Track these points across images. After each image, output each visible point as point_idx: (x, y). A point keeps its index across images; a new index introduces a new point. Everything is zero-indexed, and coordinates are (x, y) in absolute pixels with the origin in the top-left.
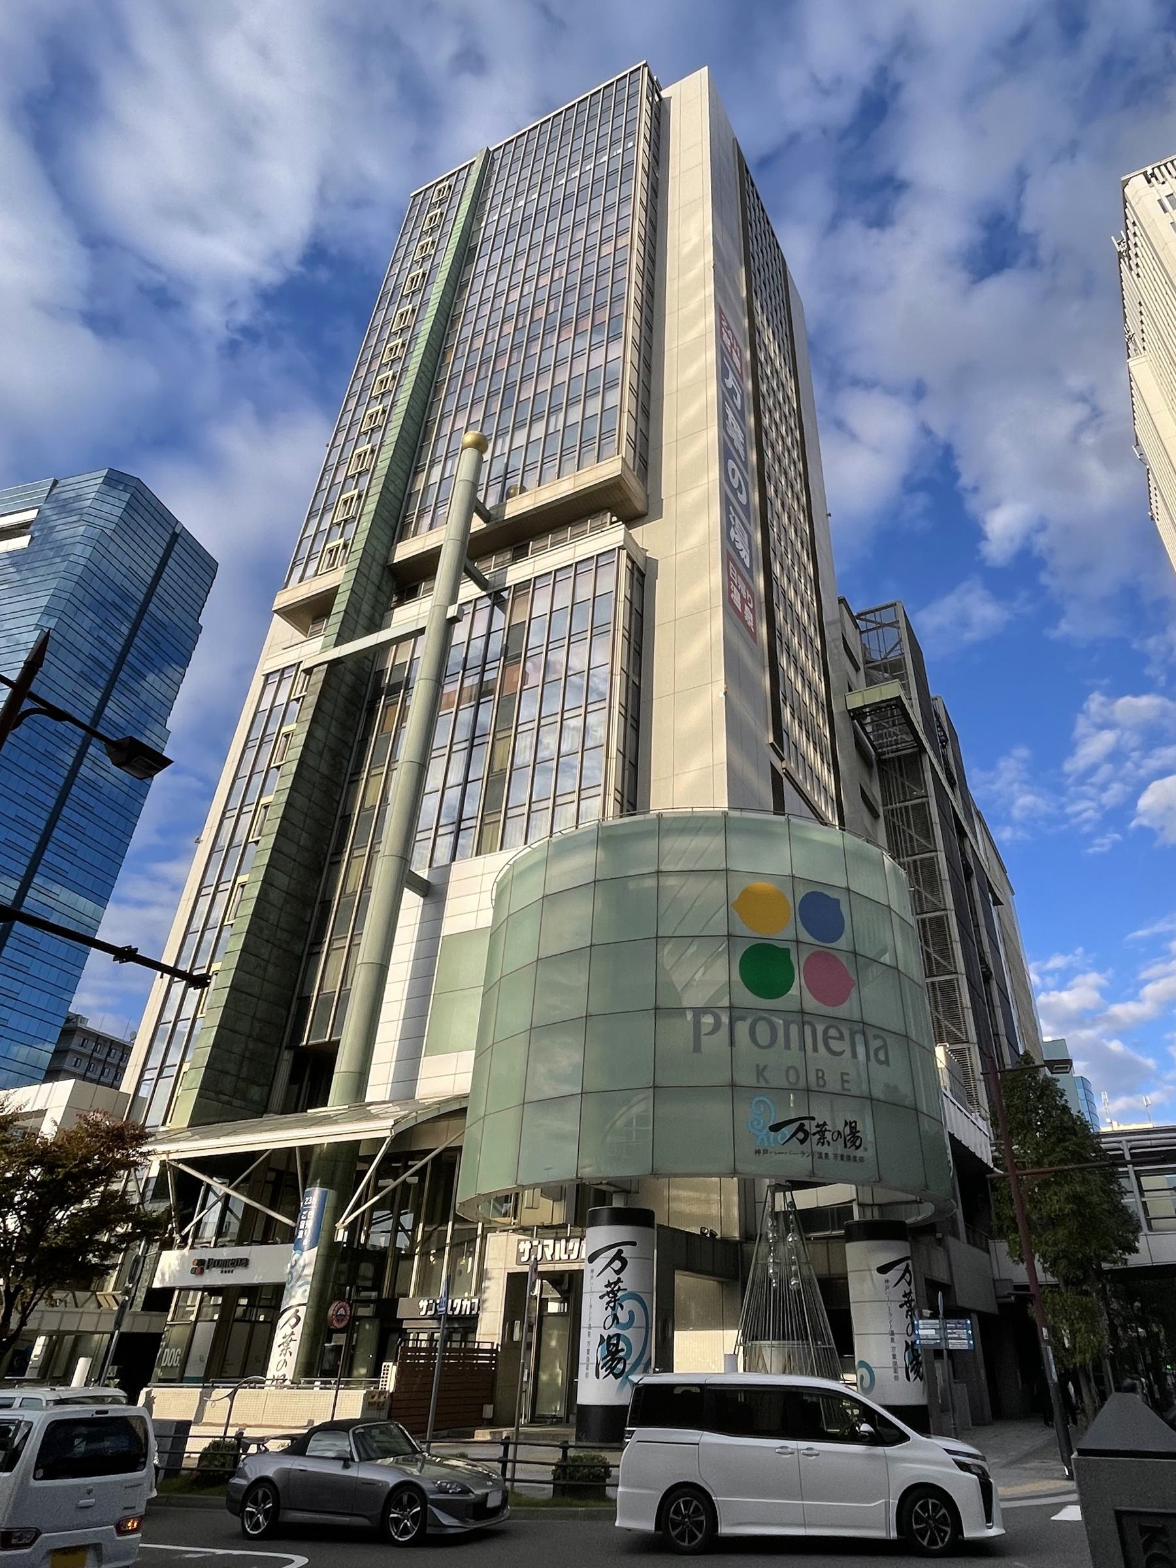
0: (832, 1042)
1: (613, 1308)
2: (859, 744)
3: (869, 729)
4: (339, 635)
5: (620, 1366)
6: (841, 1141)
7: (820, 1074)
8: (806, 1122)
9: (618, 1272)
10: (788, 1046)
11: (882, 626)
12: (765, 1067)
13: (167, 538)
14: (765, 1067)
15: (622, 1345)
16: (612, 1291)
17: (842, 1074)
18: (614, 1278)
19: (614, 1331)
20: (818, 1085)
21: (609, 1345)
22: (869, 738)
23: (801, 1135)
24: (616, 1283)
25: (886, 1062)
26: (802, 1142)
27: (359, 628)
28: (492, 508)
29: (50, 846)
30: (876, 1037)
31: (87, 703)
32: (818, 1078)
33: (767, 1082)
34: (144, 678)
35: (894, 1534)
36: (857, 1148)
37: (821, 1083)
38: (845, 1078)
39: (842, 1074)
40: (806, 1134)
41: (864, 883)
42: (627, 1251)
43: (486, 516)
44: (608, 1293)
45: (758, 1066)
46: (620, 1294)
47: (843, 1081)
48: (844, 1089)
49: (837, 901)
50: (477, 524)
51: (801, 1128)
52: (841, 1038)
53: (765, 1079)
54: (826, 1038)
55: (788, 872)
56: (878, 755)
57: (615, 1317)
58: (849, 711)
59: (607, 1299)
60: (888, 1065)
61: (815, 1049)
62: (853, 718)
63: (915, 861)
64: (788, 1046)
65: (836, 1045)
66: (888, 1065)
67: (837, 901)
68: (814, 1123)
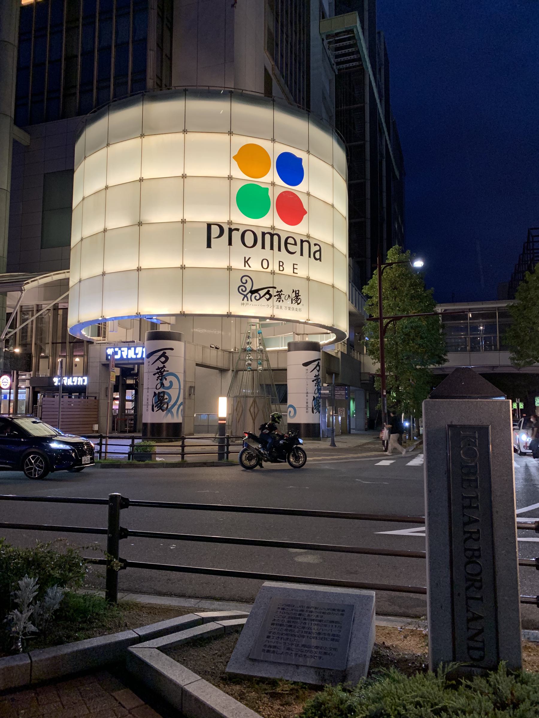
1: (161, 380)
5: (165, 406)
6: (290, 300)
7: (281, 264)
8: (271, 289)
9: (163, 363)
10: (263, 247)
15: (166, 396)
16: (160, 372)
18: (162, 365)
19: (162, 390)
21: (159, 396)
23: (163, 359)
24: (162, 368)
26: (268, 300)
30: (315, 245)
33: (250, 267)
36: (298, 304)
37: (281, 268)
40: (271, 296)
42: (168, 353)
44: (158, 373)
46: (164, 373)
51: (268, 293)
52: (295, 244)
54: (286, 243)
57: (162, 384)
59: (157, 375)
61: (279, 250)
65: (291, 248)
68: (275, 290)
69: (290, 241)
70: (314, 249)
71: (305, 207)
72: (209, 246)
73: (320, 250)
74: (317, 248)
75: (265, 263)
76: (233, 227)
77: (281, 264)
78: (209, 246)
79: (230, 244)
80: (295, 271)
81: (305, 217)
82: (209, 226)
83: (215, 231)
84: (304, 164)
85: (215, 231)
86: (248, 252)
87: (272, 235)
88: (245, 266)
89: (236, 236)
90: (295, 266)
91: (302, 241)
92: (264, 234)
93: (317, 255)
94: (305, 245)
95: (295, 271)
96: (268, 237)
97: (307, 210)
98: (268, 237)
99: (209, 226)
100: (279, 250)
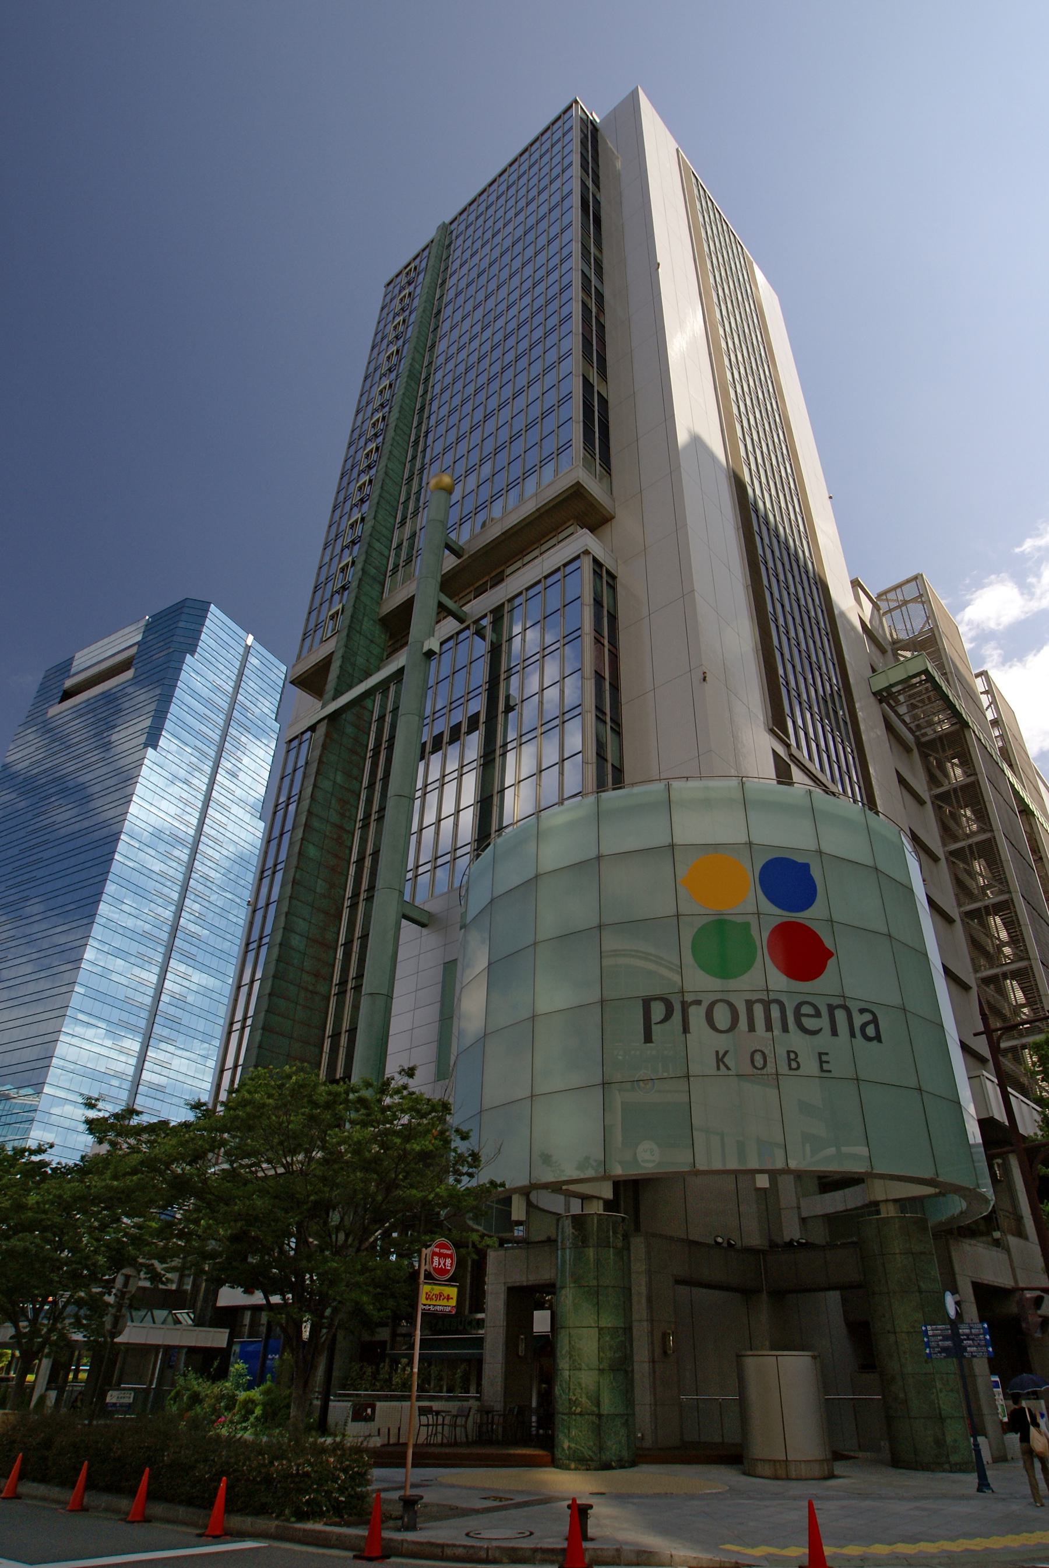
0: (805, 1021)
2: (889, 727)
3: (902, 710)
4: (336, 689)
7: (792, 1056)
10: (752, 1028)
11: (905, 603)
12: (726, 1052)
13: (241, 650)
14: (726, 1052)
17: (820, 1054)
20: (791, 1069)
22: (904, 722)
25: (878, 1038)
27: (356, 680)
28: (465, 543)
29: (169, 975)
30: (862, 1011)
31: (187, 824)
32: (789, 1060)
33: (728, 1068)
34: (110, 743)
35: (228, 1331)
37: (794, 1065)
38: (824, 1058)
39: (820, 1054)
41: (835, 842)
43: (456, 552)
45: (717, 1052)
47: (821, 1062)
48: (822, 1070)
49: (806, 866)
50: (450, 562)
52: (818, 1014)
53: (724, 1063)
55: (744, 839)
56: (917, 738)
58: (874, 694)
60: (880, 1041)
61: (785, 1029)
62: (880, 702)
63: (970, 846)
64: (752, 1028)
65: (809, 1023)
66: (880, 1041)
67: (806, 866)
69: (806, 1009)
70: (859, 1020)
71: (828, 943)
72: (648, 1038)
73: (875, 1021)
74: (867, 1017)
75: (758, 1057)
76: (689, 998)
77: (792, 1056)
78: (648, 1038)
79: (686, 1030)
80: (826, 1066)
81: (831, 963)
82: (647, 1003)
83: (658, 1011)
84: (816, 873)
85: (658, 1011)
86: (721, 1042)
87: (767, 1005)
88: (718, 1068)
89: (696, 1016)
90: (824, 1058)
91: (831, 1009)
92: (749, 1004)
93: (870, 1031)
94: (840, 1015)
95: (826, 1066)
96: (758, 1010)
97: (832, 949)
98: (758, 1010)
99: (647, 1003)
100: (785, 1029)
